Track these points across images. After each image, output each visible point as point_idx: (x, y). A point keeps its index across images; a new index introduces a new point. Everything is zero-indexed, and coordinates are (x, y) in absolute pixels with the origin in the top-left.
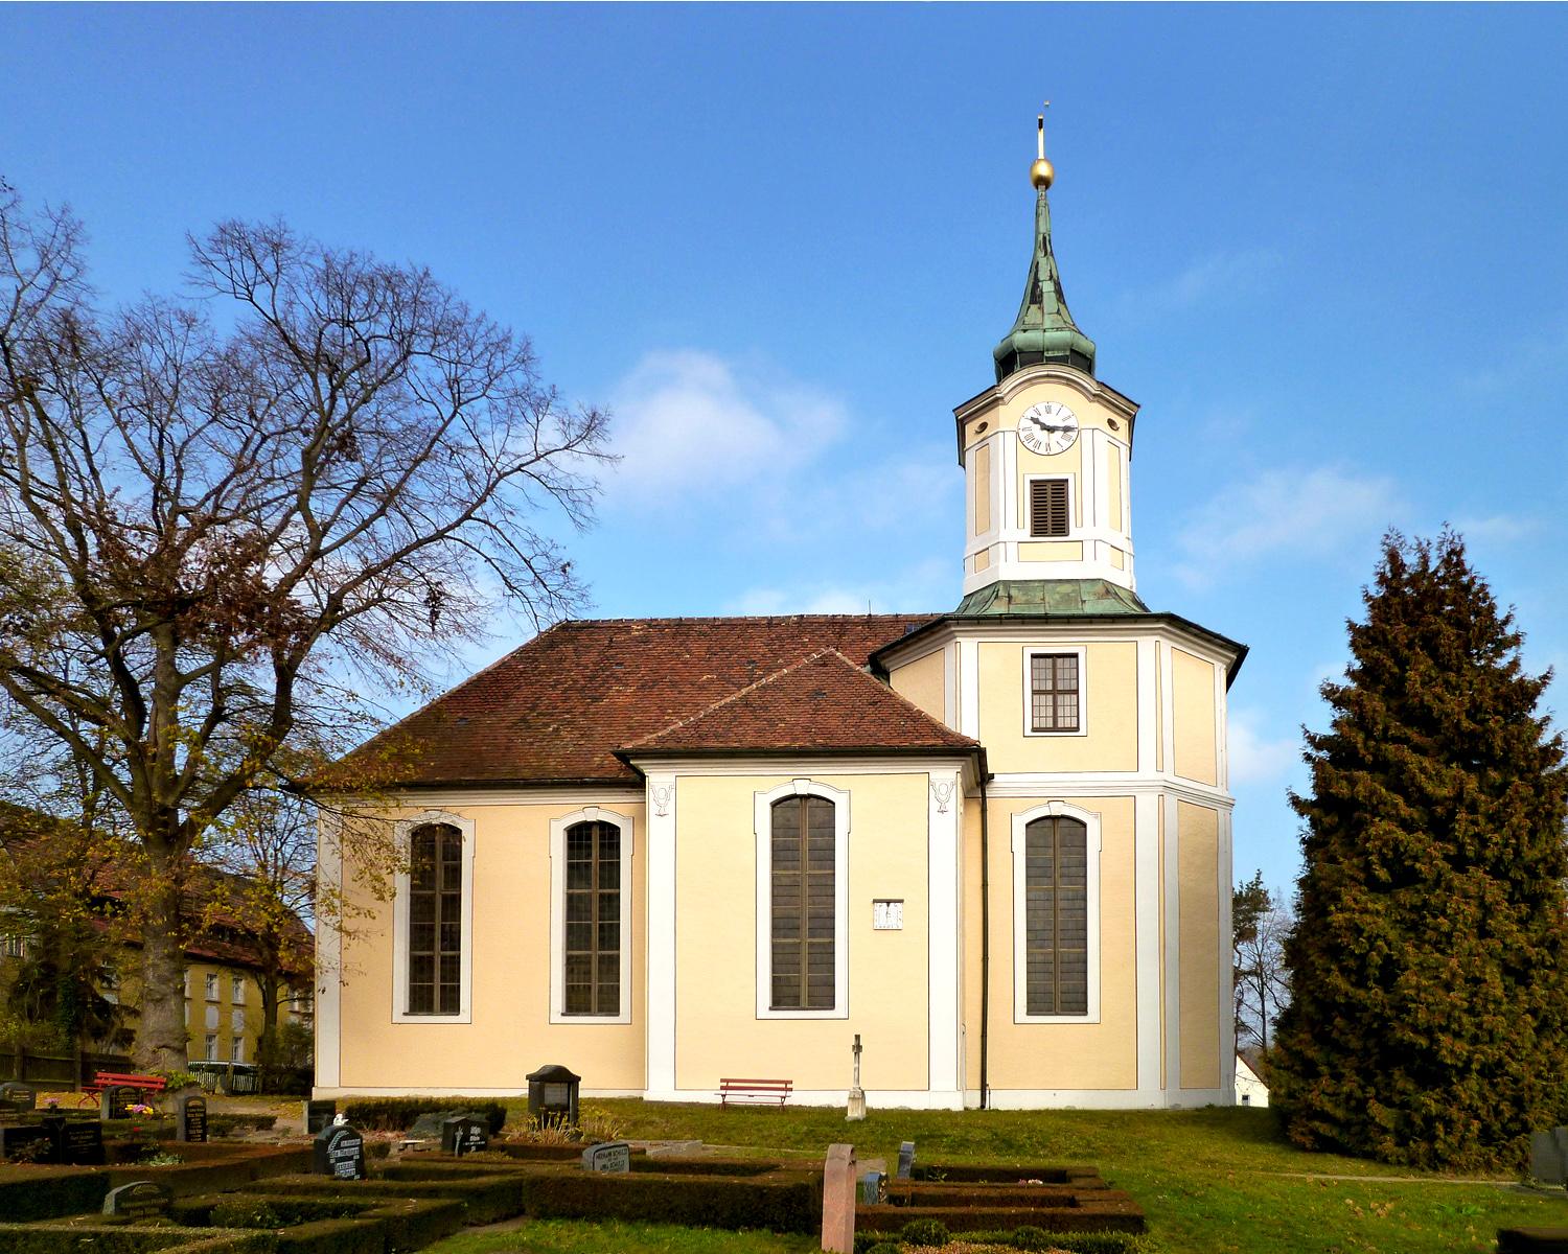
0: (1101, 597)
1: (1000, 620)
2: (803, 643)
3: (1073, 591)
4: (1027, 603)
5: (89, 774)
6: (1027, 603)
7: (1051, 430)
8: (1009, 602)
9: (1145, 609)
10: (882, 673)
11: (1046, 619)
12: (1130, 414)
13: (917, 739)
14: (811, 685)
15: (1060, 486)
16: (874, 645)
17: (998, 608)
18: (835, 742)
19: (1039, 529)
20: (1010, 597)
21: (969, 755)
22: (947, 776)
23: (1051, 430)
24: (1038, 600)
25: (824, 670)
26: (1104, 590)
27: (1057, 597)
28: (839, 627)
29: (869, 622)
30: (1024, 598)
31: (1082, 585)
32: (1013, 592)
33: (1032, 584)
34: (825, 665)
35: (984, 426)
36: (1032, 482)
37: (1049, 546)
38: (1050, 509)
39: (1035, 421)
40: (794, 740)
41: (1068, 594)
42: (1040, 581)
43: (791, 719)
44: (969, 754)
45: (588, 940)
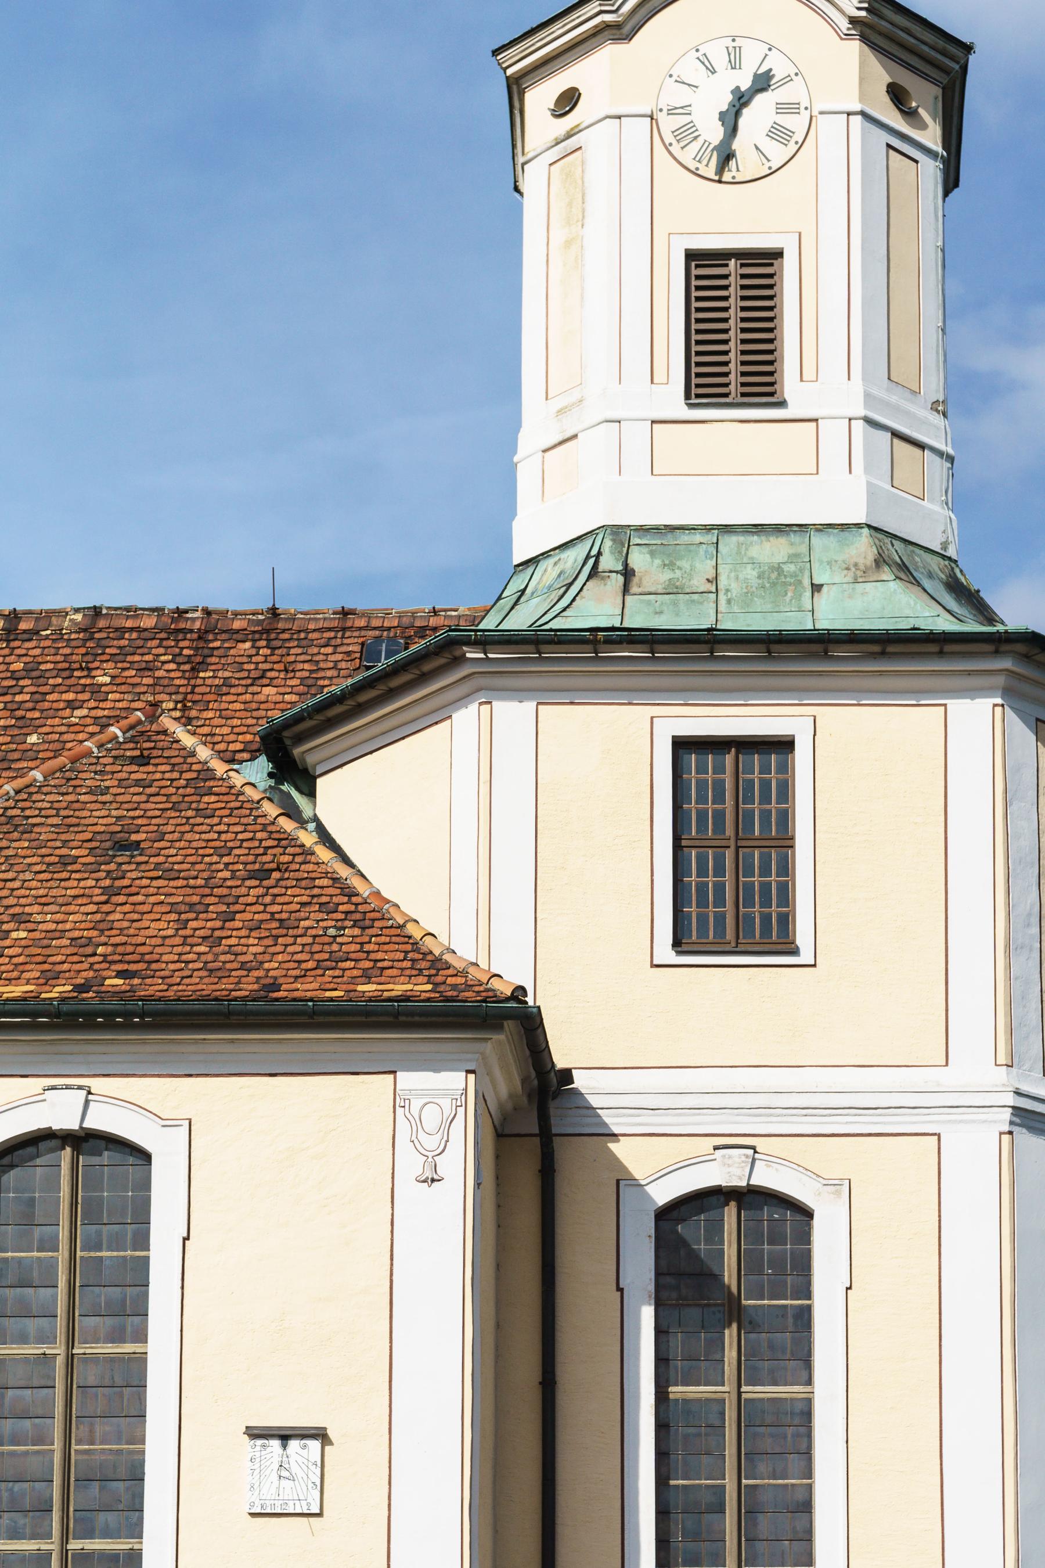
0: (860, 575)
1: (596, 641)
2: (96, 690)
3: (793, 558)
4: (673, 590)
5: (260, 617)
6: (673, 590)
7: (731, 120)
8: (626, 589)
9: (986, 614)
10: (295, 774)
11: (708, 642)
12: (946, 71)
13: (367, 977)
14: (101, 819)
15: (763, 262)
16: (279, 699)
17: (597, 609)
18: (154, 987)
19: (705, 385)
20: (628, 573)
21: (498, 1027)
22: (439, 1101)
23: (731, 120)
24: (699, 583)
25: (140, 773)
26: (871, 554)
27: (750, 573)
28: (193, 639)
29: (271, 626)
30: (667, 575)
31: (817, 540)
32: (638, 559)
33: (685, 538)
34: (143, 760)
35: (569, 100)
36: (691, 256)
37: (731, 434)
38: (731, 330)
39: (763, 83)
40: (50, 978)
41: (778, 569)
42: (708, 528)
43: (46, 919)
44: (497, 1024)
45: (792, 1253)
